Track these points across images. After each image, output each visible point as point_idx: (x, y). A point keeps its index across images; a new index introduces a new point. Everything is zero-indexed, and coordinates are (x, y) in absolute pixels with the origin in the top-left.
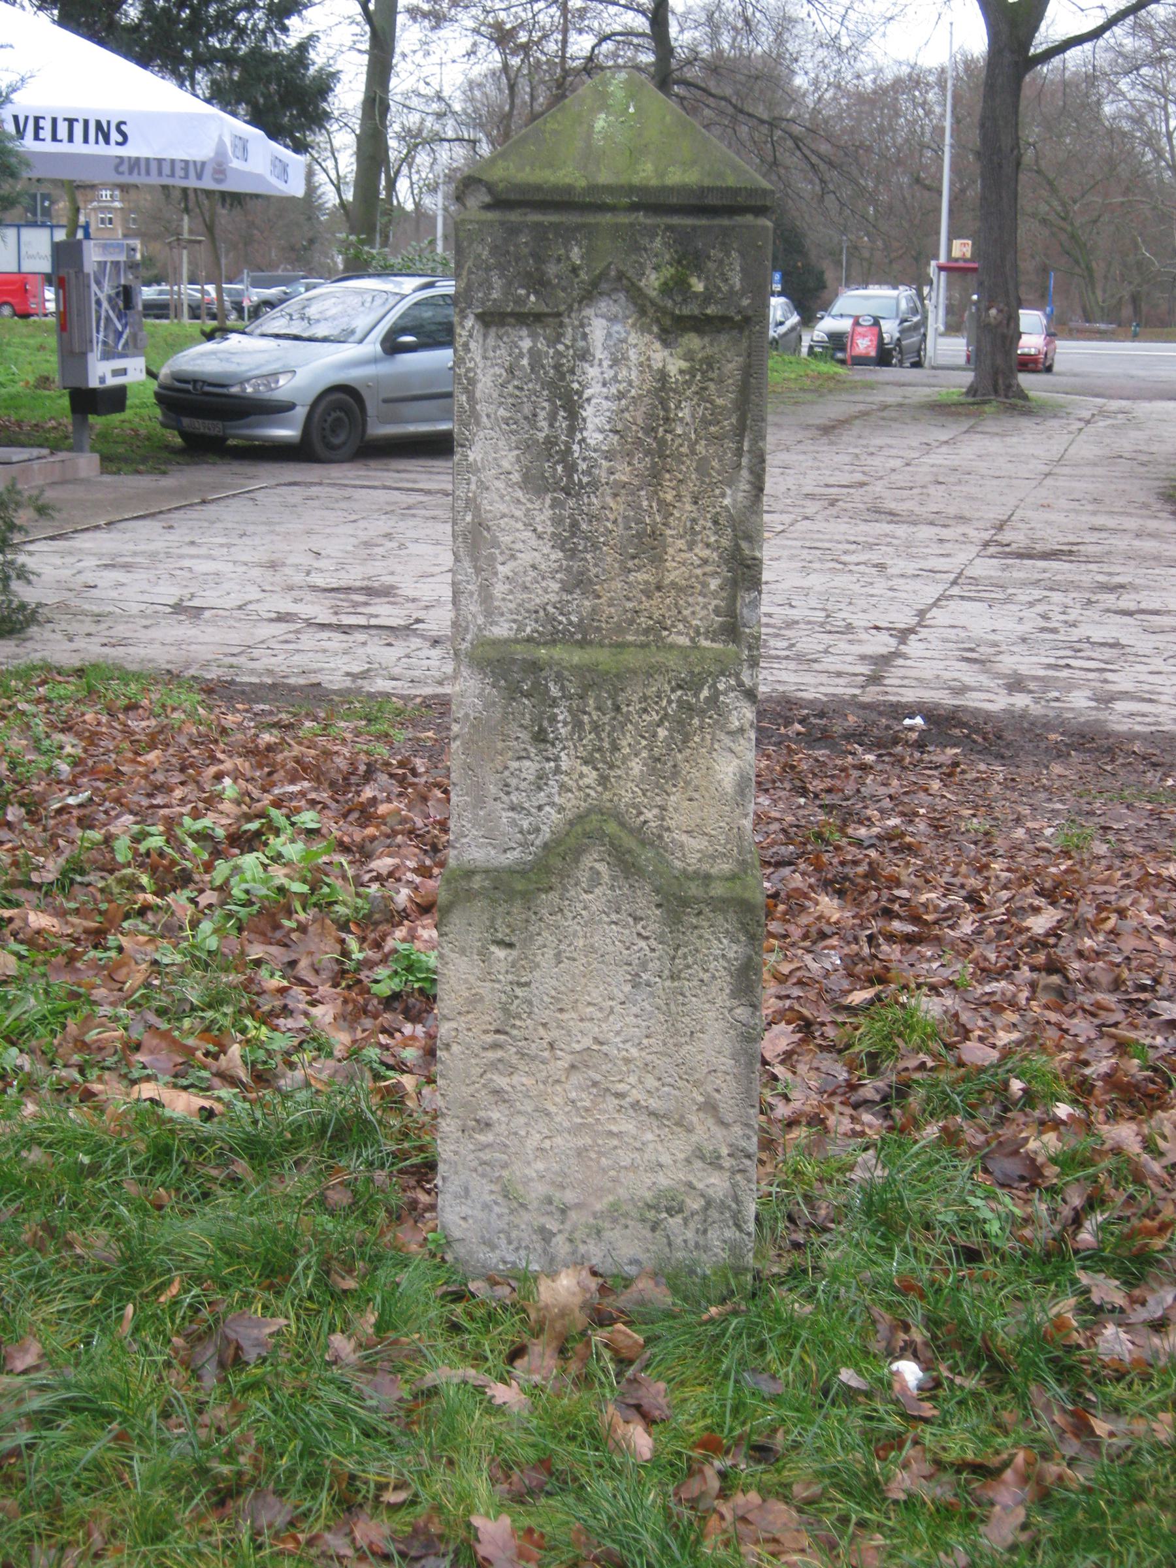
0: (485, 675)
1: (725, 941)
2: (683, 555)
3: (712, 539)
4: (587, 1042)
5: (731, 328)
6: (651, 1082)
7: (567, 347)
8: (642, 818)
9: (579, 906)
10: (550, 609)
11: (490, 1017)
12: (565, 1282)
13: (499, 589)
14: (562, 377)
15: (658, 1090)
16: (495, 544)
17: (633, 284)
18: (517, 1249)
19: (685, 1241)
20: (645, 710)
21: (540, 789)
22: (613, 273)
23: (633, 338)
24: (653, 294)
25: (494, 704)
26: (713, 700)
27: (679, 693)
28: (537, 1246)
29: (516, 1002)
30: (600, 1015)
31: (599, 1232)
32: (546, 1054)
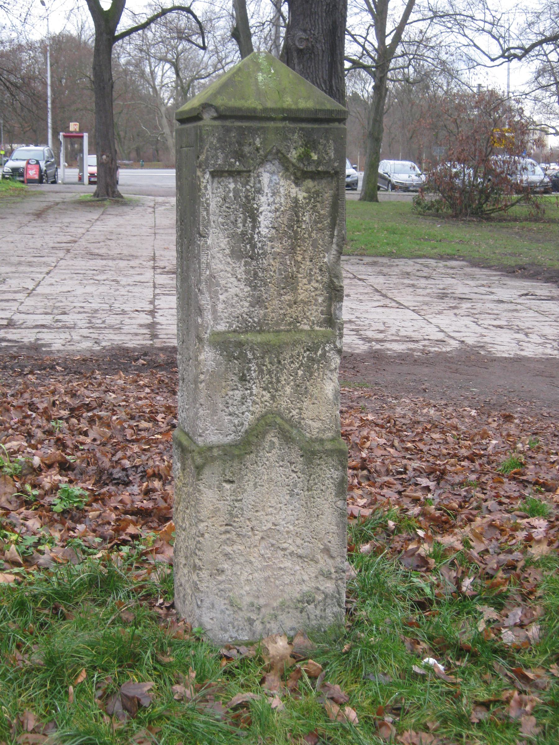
0: (217, 349)
1: (332, 470)
2: (306, 286)
3: (319, 278)
4: (270, 525)
5: (328, 177)
6: (299, 541)
7: (251, 187)
8: (291, 414)
9: (265, 459)
10: (245, 316)
11: (223, 518)
12: (281, 643)
13: (220, 307)
14: (249, 203)
15: (302, 545)
16: (218, 285)
17: (284, 156)
18: (237, 631)
19: (316, 616)
20: (292, 362)
21: (243, 404)
22: (274, 151)
23: (282, 182)
24: (294, 161)
25: (221, 364)
26: (324, 355)
27: (308, 353)
28: (247, 627)
29: (236, 509)
30: (275, 512)
31: (276, 617)
32: (250, 533)
